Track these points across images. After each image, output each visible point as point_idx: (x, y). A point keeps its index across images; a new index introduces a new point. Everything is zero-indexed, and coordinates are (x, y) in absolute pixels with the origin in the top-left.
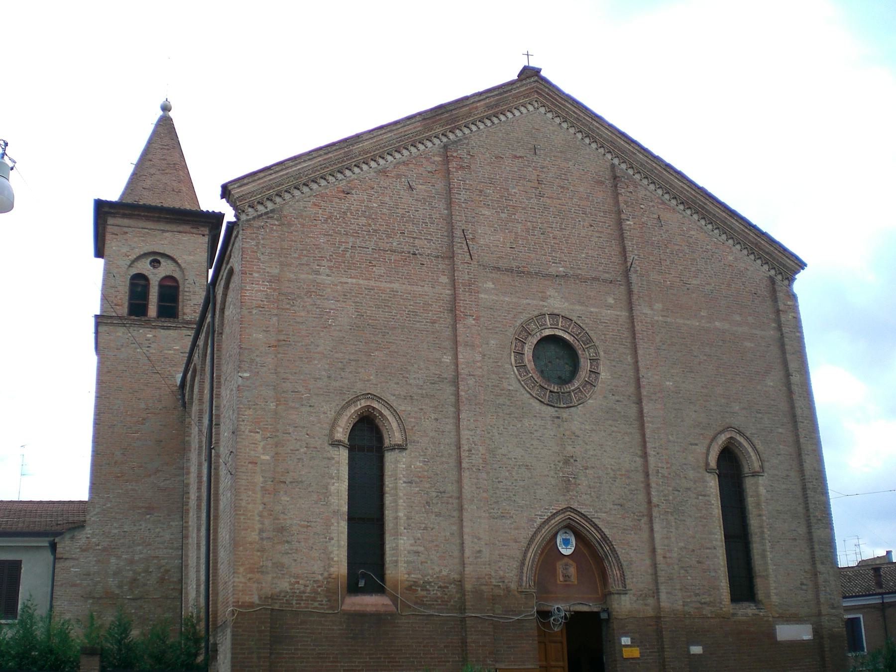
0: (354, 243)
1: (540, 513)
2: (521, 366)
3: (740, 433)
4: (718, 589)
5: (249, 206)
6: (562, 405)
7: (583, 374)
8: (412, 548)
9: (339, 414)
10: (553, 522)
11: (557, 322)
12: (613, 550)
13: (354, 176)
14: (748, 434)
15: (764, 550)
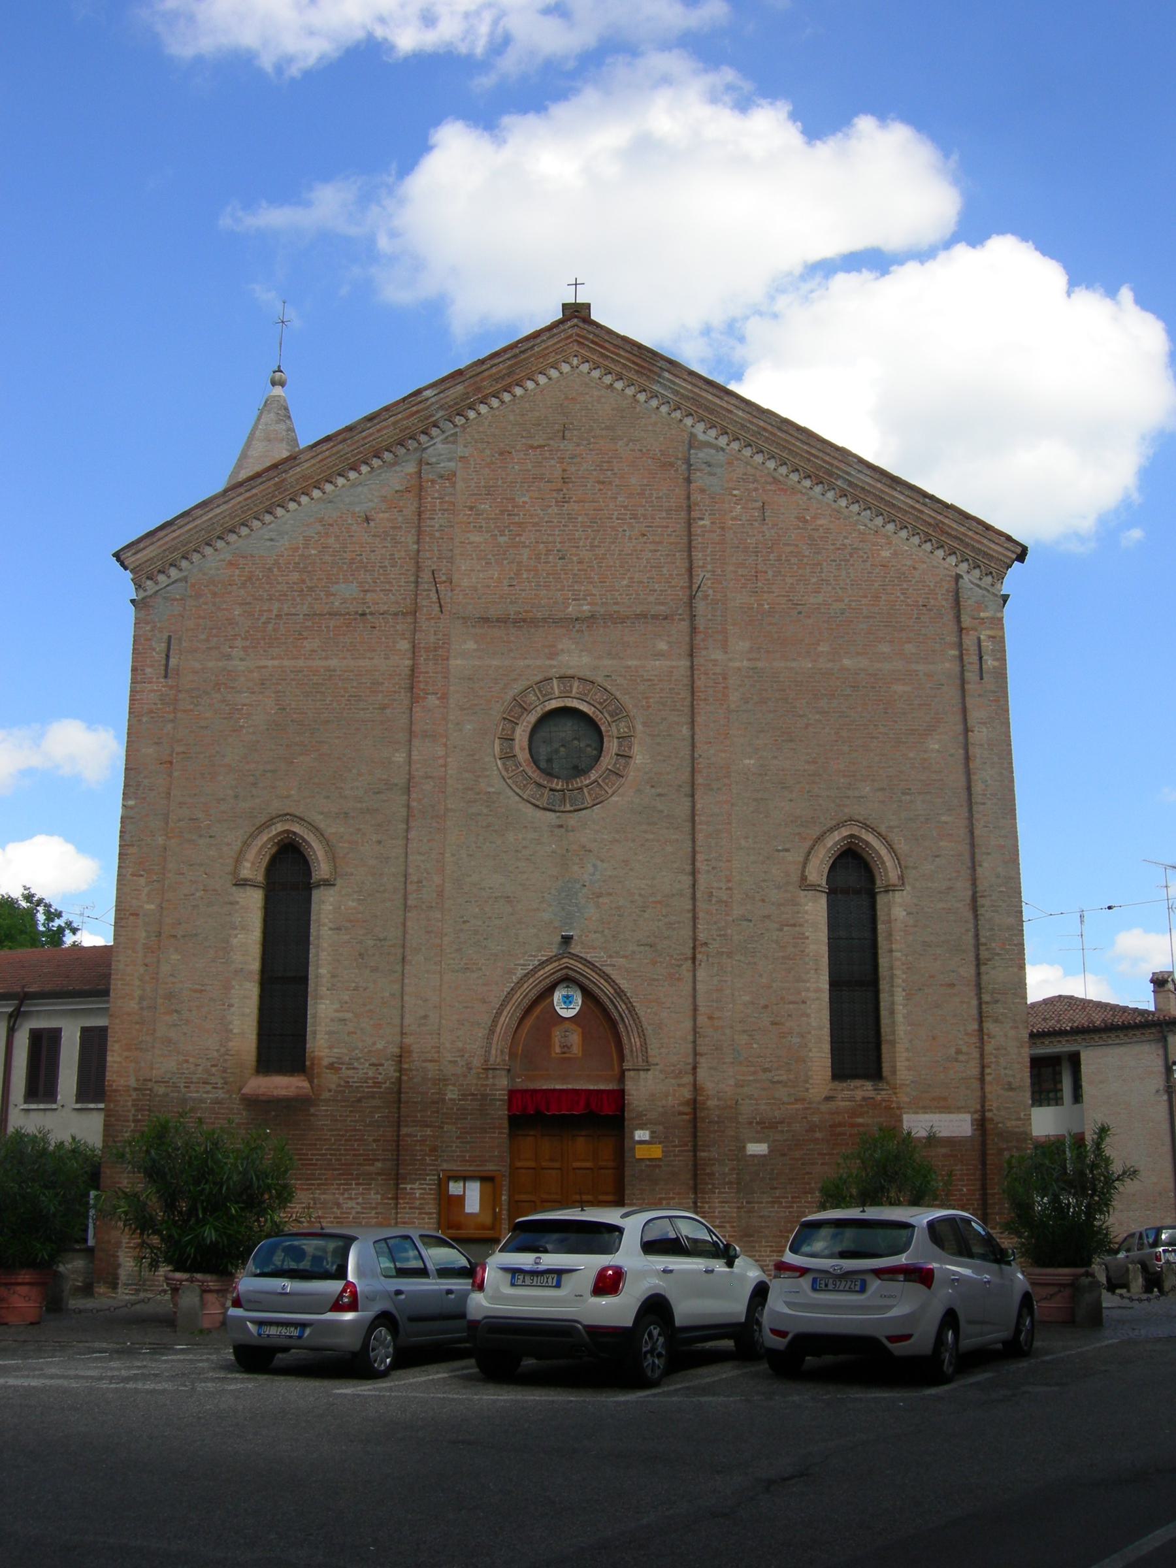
0: (280, 609)
1: (522, 962)
2: (508, 756)
3: (866, 826)
4: (804, 1061)
5: (148, 578)
6: (568, 808)
7: (606, 761)
8: (337, 1014)
9: (246, 844)
10: (541, 972)
11: (571, 687)
12: (631, 1009)
13: (288, 515)
14: (882, 829)
15: (893, 1003)
